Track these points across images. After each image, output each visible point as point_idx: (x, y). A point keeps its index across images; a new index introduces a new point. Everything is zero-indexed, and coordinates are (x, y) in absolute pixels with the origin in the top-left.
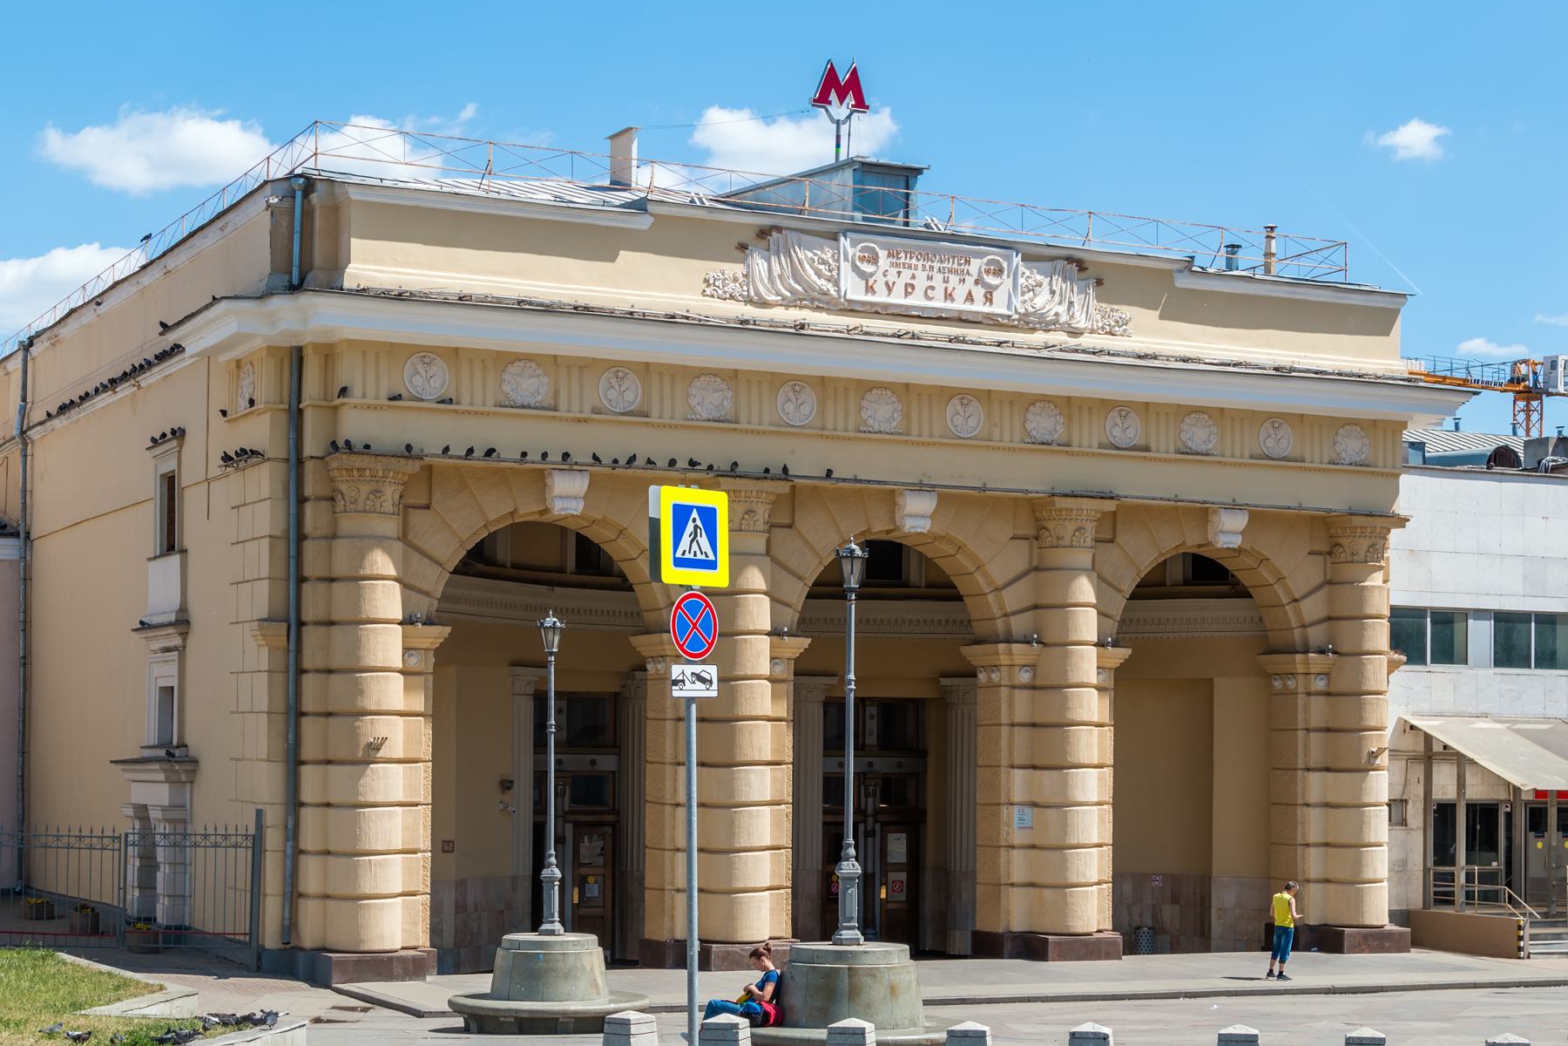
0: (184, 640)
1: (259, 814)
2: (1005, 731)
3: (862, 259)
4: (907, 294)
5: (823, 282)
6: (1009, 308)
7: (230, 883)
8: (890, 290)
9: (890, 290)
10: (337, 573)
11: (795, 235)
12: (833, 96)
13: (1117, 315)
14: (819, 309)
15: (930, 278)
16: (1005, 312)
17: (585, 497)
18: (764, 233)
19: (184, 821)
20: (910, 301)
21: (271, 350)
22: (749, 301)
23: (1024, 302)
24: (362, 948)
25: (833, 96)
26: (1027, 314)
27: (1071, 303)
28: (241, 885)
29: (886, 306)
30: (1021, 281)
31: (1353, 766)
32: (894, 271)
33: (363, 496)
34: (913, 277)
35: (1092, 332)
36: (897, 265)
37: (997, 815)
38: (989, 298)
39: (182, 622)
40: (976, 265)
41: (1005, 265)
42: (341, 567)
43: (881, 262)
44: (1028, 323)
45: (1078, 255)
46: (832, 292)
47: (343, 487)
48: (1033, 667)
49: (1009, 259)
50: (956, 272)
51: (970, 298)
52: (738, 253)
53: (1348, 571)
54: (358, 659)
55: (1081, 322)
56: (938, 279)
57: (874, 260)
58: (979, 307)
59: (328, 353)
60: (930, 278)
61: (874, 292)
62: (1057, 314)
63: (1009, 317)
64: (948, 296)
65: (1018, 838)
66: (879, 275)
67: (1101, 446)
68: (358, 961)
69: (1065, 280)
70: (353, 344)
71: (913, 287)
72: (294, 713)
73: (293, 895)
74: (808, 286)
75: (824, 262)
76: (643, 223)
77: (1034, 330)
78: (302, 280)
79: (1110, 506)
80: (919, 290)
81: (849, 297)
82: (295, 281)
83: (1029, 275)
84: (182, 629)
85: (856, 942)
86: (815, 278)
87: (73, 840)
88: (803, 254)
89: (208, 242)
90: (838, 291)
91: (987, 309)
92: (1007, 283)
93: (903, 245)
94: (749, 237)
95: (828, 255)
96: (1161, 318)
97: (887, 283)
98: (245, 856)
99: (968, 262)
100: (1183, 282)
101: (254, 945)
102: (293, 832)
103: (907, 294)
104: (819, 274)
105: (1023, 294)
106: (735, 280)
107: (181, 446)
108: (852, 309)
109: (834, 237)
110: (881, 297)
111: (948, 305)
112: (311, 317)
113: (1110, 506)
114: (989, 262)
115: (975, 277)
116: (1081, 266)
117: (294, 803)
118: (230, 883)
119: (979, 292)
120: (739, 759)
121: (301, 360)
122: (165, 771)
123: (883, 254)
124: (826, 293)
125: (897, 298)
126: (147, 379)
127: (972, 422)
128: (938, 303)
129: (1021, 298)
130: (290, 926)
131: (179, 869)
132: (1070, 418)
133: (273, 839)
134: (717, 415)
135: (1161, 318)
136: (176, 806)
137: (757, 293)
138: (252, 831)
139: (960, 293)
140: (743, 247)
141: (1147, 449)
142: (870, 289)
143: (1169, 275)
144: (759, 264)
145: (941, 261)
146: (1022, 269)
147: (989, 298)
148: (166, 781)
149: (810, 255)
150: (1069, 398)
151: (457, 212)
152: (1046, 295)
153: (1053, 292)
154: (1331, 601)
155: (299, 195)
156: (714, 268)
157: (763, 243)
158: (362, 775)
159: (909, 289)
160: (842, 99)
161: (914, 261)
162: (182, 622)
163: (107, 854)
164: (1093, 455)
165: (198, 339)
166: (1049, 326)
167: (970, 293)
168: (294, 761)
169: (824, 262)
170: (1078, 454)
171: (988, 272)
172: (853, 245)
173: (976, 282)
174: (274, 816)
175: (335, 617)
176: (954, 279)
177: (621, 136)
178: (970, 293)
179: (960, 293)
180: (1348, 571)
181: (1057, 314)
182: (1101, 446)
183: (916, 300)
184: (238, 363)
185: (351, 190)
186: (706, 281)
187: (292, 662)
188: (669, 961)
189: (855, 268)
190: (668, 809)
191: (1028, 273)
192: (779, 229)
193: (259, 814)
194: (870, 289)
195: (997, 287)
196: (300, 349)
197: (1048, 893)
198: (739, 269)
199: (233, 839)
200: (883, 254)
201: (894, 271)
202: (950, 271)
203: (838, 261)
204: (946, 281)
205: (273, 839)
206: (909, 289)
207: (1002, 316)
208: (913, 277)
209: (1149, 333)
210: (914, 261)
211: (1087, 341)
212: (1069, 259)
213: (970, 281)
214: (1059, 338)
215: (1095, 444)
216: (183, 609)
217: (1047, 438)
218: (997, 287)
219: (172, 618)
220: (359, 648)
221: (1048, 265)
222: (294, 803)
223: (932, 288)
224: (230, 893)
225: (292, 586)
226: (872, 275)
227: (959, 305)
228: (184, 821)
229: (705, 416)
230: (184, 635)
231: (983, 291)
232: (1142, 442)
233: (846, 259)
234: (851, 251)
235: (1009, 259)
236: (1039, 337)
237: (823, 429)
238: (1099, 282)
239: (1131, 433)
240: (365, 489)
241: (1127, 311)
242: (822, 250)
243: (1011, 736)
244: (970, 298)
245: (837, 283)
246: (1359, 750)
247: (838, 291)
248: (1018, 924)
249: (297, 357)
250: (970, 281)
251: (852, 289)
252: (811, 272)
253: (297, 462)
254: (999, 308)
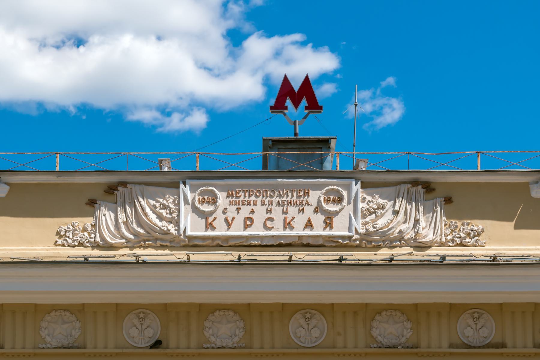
3: (202, 202)
4: (246, 227)
5: (165, 223)
6: (350, 230)
8: (229, 225)
9: (229, 225)
11: (138, 187)
12: (289, 103)
13: (468, 228)
14: (162, 247)
15: (269, 211)
16: (346, 233)
18: (111, 190)
20: (249, 232)
22: (95, 246)
23: (366, 223)
25: (289, 103)
26: (368, 234)
27: (417, 221)
30: (361, 205)
32: (234, 208)
34: (252, 212)
35: (441, 244)
36: (236, 203)
38: (328, 224)
40: (314, 196)
41: (345, 193)
43: (220, 202)
44: (368, 241)
45: (424, 177)
46: (173, 230)
49: (348, 188)
50: (295, 204)
51: (309, 225)
52: (88, 208)
55: (427, 234)
56: (277, 213)
57: (214, 200)
58: (319, 231)
60: (269, 211)
61: (213, 228)
62: (400, 232)
63: (350, 238)
64: (287, 225)
66: (219, 214)
67: (451, 346)
69: (409, 201)
71: (251, 220)
74: (150, 229)
75: (165, 207)
77: (379, 247)
81: (189, 233)
83: (368, 200)
86: (157, 222)
88: (145, 205)
90: (178, 230)
91: (327, 232)
92: (349, 209)
93: (242, 186)
95: (169, 201)
96: (516, 227)
97: (226, 220)
99: (307, 194)
103: (246, 227)
104: (160, 217)
105: (364, 217)
106: (85, 230)
108: (194, 244)
110: (221, 231)
111: (288, 232)
114: (327, 193)
115: (315, 205)
116: (428, 188)
119: (318, 220)
123: (221, 196)
124: (167, 233)
125: (237, 231)
127: (316, 333)
128: (278, 231)
129: (361, 221)
134: (65, 343)
135: (516, 227)
137: (103, 238)
139: (299, 221)
140: (92, 203)
142: (209, 226)
144: (106, 216)
145: (280, 196)
146: (361, 194)
147: (328, 224)
149: (152, 202)
150: (416, 305)
153: (396, 213)
156: (64, 223)
157: (111, 198)
159: (248, 222)
160: (296, 104)
161: (253, 198)
164: (445, 354)
166: (391, 242)
167: (309, 220)
169: (165, 207)
170: (429, 355)
171: (327, 201)
172: (193, 191)
173: (316, 211)
176: (293, 210)
177: (161, 161)
178: (309, 220)
179: (299, 221)
181: (400, 232)
182: (451, 346)
183: (256, 231)
186: (58, 233)
189: (195, 210)
191: (369, 198)
192: (124, 184)
194: (209, 226)
195: (337, 213)
198: (89, 221)
200: (221, 196)
201: (234, 208)
202: (289, 203)
203: (178, 204)
204: (285, 212)
206: (248, 222)
207: (343, 237)
208: (252, 212)
210: (253, 198)
211: (435, 252)
212: (415, 183)
213: (309, 211)
214: (403, 253)
215: (445, 344)
217: (394, 342)
218: (337, 213)
221: (391, 190)
223: (271, 219)
226: (211, 213)
227: (299, 231)
229: (55, 344)
231: (323, 218)
232: (498, 340)
233: (186, 202)
234: (190, 196)
235: (348, 188)
236: (384, 254)
238: (448, 200)
239: (484, 332)
241: (478, 224)
242: (164, 198)
244: (309, 225)
245: (177, 224)
247: (178, 230)
251: (191, 225)
252: (153, 217)
254: (340, 230)
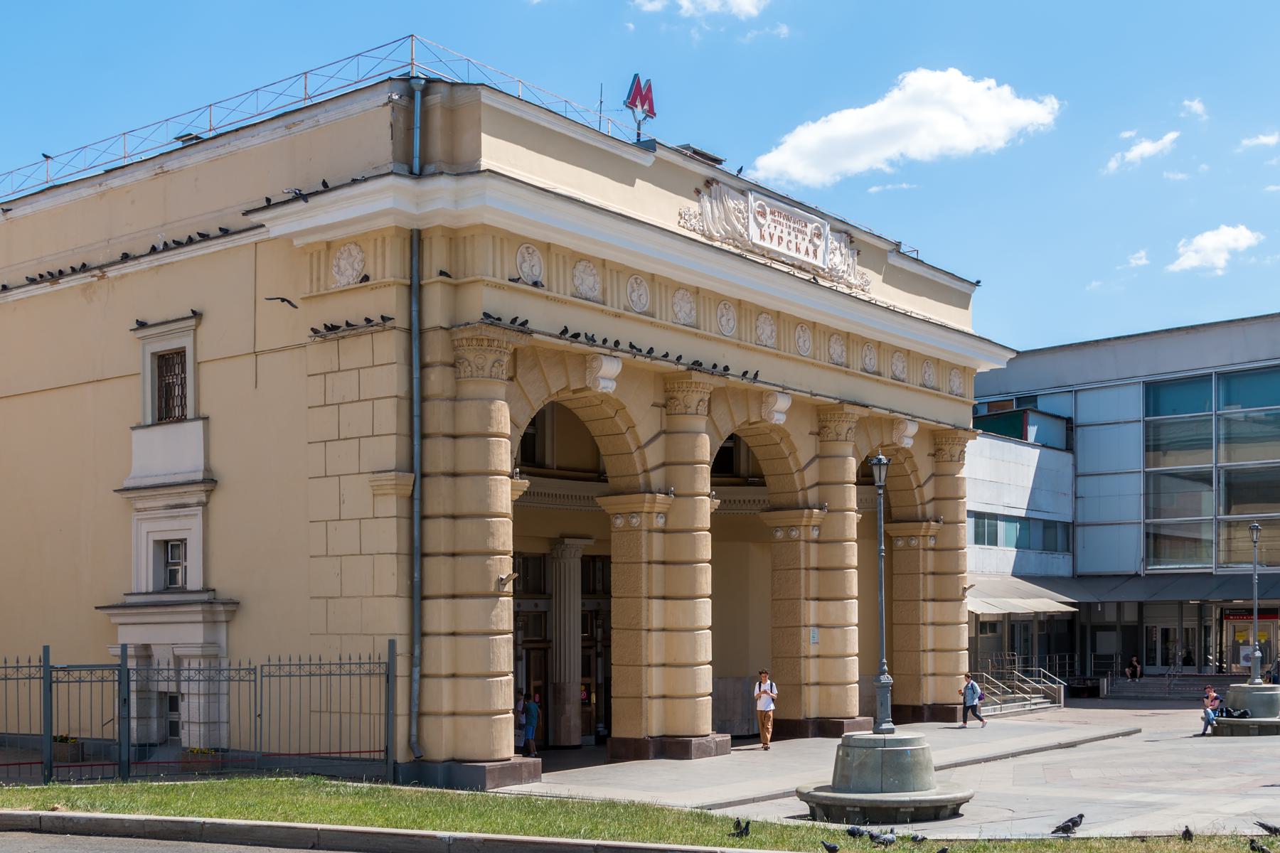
0: (208, 497)
1: (392, 644)
2: (803, 572)
7: (356, 708)
10: (462, 429)
11: (725, 188)
16: (821, 265)
17: (616, 379)
18: (709, 183)
19: (216, 657)
21: (398, 229)
22: (703, 235)
24: (496, 757)
28: (375, 710)
29: (769, 251)
31: (953, 597)
33: (489, 364)
37: (799, 635)
39: (210, 482)
42: (468, 423)
47: (471, 356)
48: (819, 527)
52: (694, 195)
53: (947, 468)
54: (489, 505)
59: (454, 237)
64: (798, 250)
65: (656, 658)
68: (502, 768)
70: (485, 228)
72: (416, 555)
73: (417, 714)
76: (646, 159)
78: (421, 169)
79: (865, 412)
80: (784, 243)
82: (416, 169)
84: (209, 487)
85: (891, 731)
87: (233, 673)
89: (255, 141)
94: (701, 185)
98: (378, 683)
100: (894, 260)
101: (391, 761)
102: (416, 659)
104: (738, 219)
107: (197, 326)
109: (743, 193)
112: (438, 200)
113: (865, 412)
117: (418, 633)
118: (365, 709)
120: (699, 593)
121: (420, 241)
122: (203, 611)
126: (64, 283)
130: (415, 743)
131: (212, 698)
132: (848, 348)
133: (402, 667)
136: (208, 643)
138: (385, 659)
140: (698, 192)
141: (879, 374)
143: (883, 253)
148: (204, 622)
151: (544, 128)
152: (833, 256)
154: (936, 487)
155: (418, 95)
158: (494, 607)
162: (210, 482)
163: (244, 685)
165: (660, 152)
168: (417, 595)
172: (756, 200)
174: (402, 647)
175: (462, 468)
180: (947, 468)
184: (329, 245)
185: (484, 93)
187: (417, 508)
188: (651, 754)
189: (756, 219)
190: (644, 633)
192: (718, 182)
193: (392, 644)
194: (762, 237)
196: (419, 232)
197: (834, 689)
199: (165, 673)
201: (773, 225)
205: (402, 667)
209: (881, 291)
216: (207, 469)
219: (200, 476)
220: (489, 496)
222: (418, 633)
224: (325, 717)
225: (416, 442)
228: (216, 657)
230: (209, 493)
237: (740, 339)
240: (491, 357)
243: (807, 576)
244: (807, 253)
246: (958, 587)
248: (813, 713)
249: (416, 240)
250: (807, 239)
253: (416, 333)
